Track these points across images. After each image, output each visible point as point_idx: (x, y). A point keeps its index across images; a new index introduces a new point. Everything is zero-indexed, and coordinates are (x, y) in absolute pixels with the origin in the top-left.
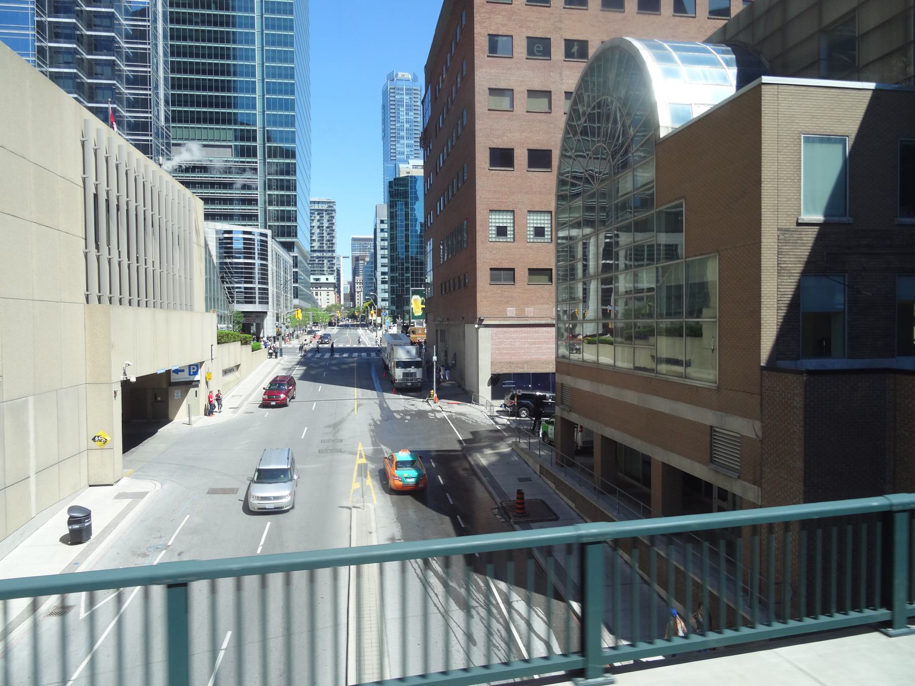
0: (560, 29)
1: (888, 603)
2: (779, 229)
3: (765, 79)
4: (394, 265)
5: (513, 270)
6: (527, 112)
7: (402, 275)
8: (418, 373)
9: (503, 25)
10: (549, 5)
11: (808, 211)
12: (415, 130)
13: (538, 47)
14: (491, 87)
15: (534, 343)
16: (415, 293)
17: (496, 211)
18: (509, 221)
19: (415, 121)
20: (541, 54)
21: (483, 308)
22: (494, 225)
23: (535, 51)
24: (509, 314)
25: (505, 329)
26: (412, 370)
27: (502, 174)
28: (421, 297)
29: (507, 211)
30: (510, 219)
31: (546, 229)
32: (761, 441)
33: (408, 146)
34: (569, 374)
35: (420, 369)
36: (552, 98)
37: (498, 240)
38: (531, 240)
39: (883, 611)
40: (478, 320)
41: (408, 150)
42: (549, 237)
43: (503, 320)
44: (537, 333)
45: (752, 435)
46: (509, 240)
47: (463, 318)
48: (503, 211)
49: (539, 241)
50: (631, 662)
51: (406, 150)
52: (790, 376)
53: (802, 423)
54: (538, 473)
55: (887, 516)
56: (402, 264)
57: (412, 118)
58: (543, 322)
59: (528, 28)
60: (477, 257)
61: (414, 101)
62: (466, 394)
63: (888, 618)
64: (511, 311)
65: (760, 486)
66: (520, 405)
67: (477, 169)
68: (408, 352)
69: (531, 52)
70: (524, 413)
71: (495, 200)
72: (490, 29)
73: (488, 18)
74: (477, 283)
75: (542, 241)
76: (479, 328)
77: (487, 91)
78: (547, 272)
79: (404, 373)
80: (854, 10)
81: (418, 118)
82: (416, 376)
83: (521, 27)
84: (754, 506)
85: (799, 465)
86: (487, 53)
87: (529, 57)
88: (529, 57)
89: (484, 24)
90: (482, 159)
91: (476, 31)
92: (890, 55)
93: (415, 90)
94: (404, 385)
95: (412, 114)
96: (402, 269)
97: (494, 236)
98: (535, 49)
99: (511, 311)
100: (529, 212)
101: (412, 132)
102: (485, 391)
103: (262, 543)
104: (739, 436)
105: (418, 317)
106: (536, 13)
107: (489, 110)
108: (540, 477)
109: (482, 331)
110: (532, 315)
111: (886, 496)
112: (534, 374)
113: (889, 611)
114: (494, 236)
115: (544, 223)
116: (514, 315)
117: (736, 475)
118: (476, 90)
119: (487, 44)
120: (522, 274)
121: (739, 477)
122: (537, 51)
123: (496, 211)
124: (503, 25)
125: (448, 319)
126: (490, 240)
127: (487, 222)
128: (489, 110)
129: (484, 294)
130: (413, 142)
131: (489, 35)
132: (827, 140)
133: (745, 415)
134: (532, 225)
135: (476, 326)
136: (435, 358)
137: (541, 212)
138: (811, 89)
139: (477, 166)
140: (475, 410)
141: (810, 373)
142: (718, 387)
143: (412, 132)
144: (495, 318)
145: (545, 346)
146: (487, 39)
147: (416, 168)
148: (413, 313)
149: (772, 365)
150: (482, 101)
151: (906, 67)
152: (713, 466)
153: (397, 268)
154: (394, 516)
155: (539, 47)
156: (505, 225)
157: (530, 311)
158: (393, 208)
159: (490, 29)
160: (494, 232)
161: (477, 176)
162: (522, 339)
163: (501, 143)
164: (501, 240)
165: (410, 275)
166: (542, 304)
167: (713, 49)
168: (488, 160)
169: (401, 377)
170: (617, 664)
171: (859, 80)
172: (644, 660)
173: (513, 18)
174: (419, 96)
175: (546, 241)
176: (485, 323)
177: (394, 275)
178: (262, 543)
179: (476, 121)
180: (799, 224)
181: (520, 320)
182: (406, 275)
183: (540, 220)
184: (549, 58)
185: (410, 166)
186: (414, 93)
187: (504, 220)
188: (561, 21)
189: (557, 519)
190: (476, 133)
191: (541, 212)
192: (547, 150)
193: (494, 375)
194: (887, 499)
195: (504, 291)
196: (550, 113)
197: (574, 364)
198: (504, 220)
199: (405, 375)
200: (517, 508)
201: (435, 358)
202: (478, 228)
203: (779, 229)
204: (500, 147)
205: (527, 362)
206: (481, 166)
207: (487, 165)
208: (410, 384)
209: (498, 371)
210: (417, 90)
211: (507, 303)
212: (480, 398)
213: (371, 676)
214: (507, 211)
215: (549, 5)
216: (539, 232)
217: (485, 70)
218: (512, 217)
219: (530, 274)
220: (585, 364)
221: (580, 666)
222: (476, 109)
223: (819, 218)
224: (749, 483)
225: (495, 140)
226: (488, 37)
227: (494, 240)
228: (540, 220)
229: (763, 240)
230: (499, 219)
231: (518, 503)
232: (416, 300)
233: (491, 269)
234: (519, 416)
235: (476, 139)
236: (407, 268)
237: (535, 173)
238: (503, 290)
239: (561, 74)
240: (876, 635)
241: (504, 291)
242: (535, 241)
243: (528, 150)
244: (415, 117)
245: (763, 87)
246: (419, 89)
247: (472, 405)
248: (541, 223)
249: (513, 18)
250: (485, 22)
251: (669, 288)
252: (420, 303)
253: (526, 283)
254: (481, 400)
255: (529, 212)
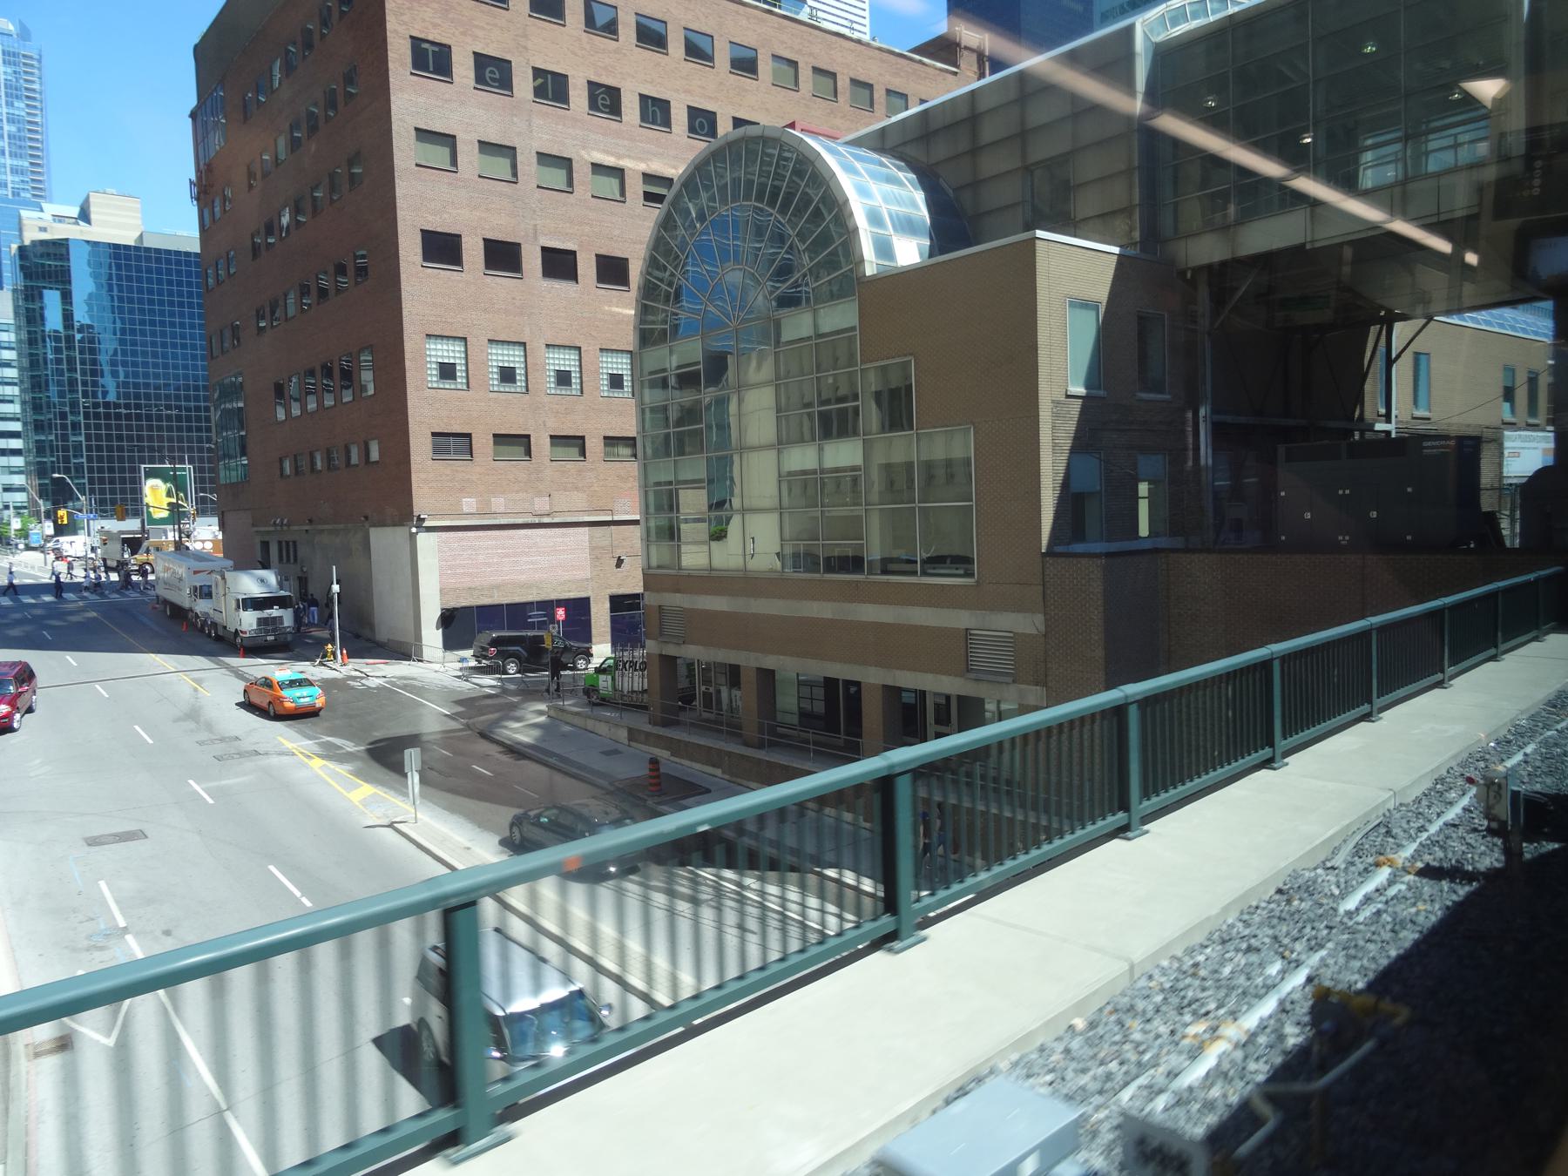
0: (525, 48)
1: (1124, 806)
2: (1053, 402)
3: (1040, 233)
4: (42, 418)
5: (469, 436)
6: (480, 176)
7: (65, 438)
8: (287, 617)
9: (435, 26)
10: (505, 6)
11: (1073, 385)
12: (31, 139)
13: (491, 72)
14: (421, 127)
15: (507, 556)
16: (151, 474)
17: (437, 337)
18: (572, 363)
19: (29, 122)
20: (607, 110)
21: (423, 499)
22: (495, 364)
23: (488, 79)
24: (466, 509)
25: (460, 534)
26: (275, 612)
27: (441, 276)
28: (165, 481)
29: (455, 338)
30: (519, 356)
31: (458, 368)
32: (1045, 636)
33: (15, 171)
34: (678, 591)
35: (290, 610)
36: (518, 159)
37: (441, 386)
38: (496, 389)
39: (1121, 815)
40: (415, 519)
41: (17, 179)
42: (524, 384)
43: (458, 519)
44: (511, 538)
45: (1031, 631)
46: (459, 387)
47: (366, 518)
48: (559, 346)
49: (507, 390)
50: (681, 1029)
51: (10, 178)
52: (1084, 561)
53: (1101, 609)
54: (626, 742)
55: (1265, 666)
56: (63, 416)
57: (23, 114)
58: (520, 521)
59: (475, 38)
60: (409, 413)
61: (26, 80)
62: (404, 651)
63: (891, 928)
64: (469, 504)
65: (1045, 684)
66: (504, 656)
67: (402, 264)
68: (262, 581)
69: (540, 92)
70: (512, 668)
71: (434, 318)
72: (413, 27)
73: (408, 8)
74: (412, 458)
75: (513, 390)
76: (417, 533)
77: (413, 133)
78: (630, 442)
79: (259, 619)
80: (1068, 153)
81: (35, 115)
82: (282, 623)
83: (463, 34)
84: (1036, 708)
85: (1099, 653)
86: (409, 67)
87: (479, 87)
88: (479, 87)
89: (404, 18)
90: (410, 249)
91: (389, 26)
92: (1113, 213)
93: (24, 56)
94: (260, 641)
95: (22, 105)
96: (64, 427)
97: (435, 379)
98: (488, 75)
99: (469, 504)
100: (429, 336)
101: (23, 144)
102: (432, 637)
103: (298, 893)
104: (1011, 635)
105: (162, 521)
106: (486, 15)
107: (417, 165)
108: (629, 746)
109: (423, 539)
110: (502, 509)
111: (1122, 687)
112: (510, 606)
113: (894, 918)
114: (435, 379)
115: (514, 362)
116: (474, 511)
117: (1009, 679)
118: (394, 127)
119: (409, 53)
120: (594, 445)
121: (1014, 682)
122: (602, 104)
123: (437, 337)
124: (435, 26)
125: (311, 521)
126: (430, 385)
127: (485, 363)
128: (417, 165)
129: (423, 476)
130: (26, 164)
131: (411, 37)
132: (1085, 305)
133: (1019, 608)
134: (552, 367)
135: (414, 530)
136: (336, 588)
137: (509, 343)
138: (1100, 254)
139: (401, 258)
140: (421, 670)
141: (1109, 555)
142: (977, 582)
143: (23, 144)
144: (443, 516)
145: (525, 559)
146: (408, 44)
147: (60, 221)
148: (149, 514)
149: (1050, 553)
150: (405, 150)
151: (1131, 231)
152: (973, 675)
153: (50, 424)
154: (470, 825)
155: (605, 99)
156: (452, 361)
157: (498, 503)
158: (33, 301)
159: (413, 27)
160: (434, 372)
161: (403, 276)
162: (487, 549)
163: (441, 223)
164: (447, 386)
165: (82, 438)
166: (517, 492)
167: (891, 163)
168: (419, 250)
169: (255, 627)
170: (932, 914)
171: (1075, 236)
172: (696, 1022)
173: (450, 16)
174: (36, 71)
175: (519, 390)
176: (426, 524)
177: (43, 438)
178: (298, 893)
179: (397, 181)
180: (1068, 396)
181: (599, 515)
182: (72, 438)
183: (508, 355)
184: (510, 93)
185: (47, 216)
186: (25, 64)
187: (513, 357)
188: (525, 36)
189: (708, 791)
190: (398, 201)
191: (509, 343)
192: (623, 259)
193: (448, 610)
194: (1122, 691)
195: (457, 471)
196: (516, 183)
197: (689, 576)
198: (449, 352)
199: (261, 621)
200: (651, 784)
201: (336, 588)
202: (407, 363)
203: (1053, 402)
204: (439, 230)
205: (498, 587)
206: (409, 259)
207: (419, 258)
208: (272, 638)
209: (452, 604)
210: (31, 58)
211: (462, 490)
212: (425, 649)
213: (292, 1154)
214: (455, 338)
215: (505, 6)
216: (616, 381)
217: (406, 96)
218: (463, 349)
219: (495, 443)
220: (714, 574)
221: (449, 1129)
222: (396, 161)
223: (1080, 390)
224: (1028, 684)
225: (430, 218)
226: (410, 40)
227: (435, 385)
228: (508, 355)
229: (1041, 413)
230: (503, 355)
231: (651, 777)
232: (154, 488)
233: (434, 434)
234: (506, 673)
235: (398, 211)
236: (75, 426)
237: (497, 278)
238: (453, 469)
239: (529, 121)
240: (1116, 841)
241: (457, 471)
242: (502, 389)
243: (484, 239)
244: (28, 114)
245: (1037, 241)
246: (36, 57)
247: (412, 663)
248: (508, 361)
249: (450, 16)
250: (405, 14)
251: (888, 468)
252: (164, 493)
253: (491, 458)
254: (427, 653)
255: (490, 341)
